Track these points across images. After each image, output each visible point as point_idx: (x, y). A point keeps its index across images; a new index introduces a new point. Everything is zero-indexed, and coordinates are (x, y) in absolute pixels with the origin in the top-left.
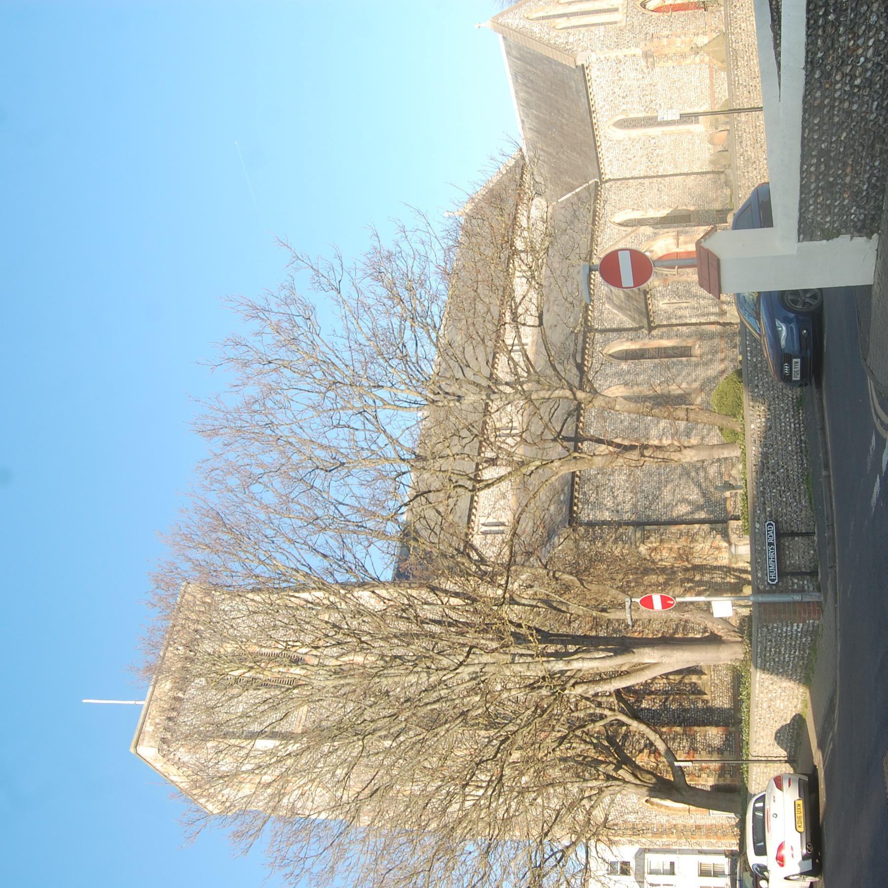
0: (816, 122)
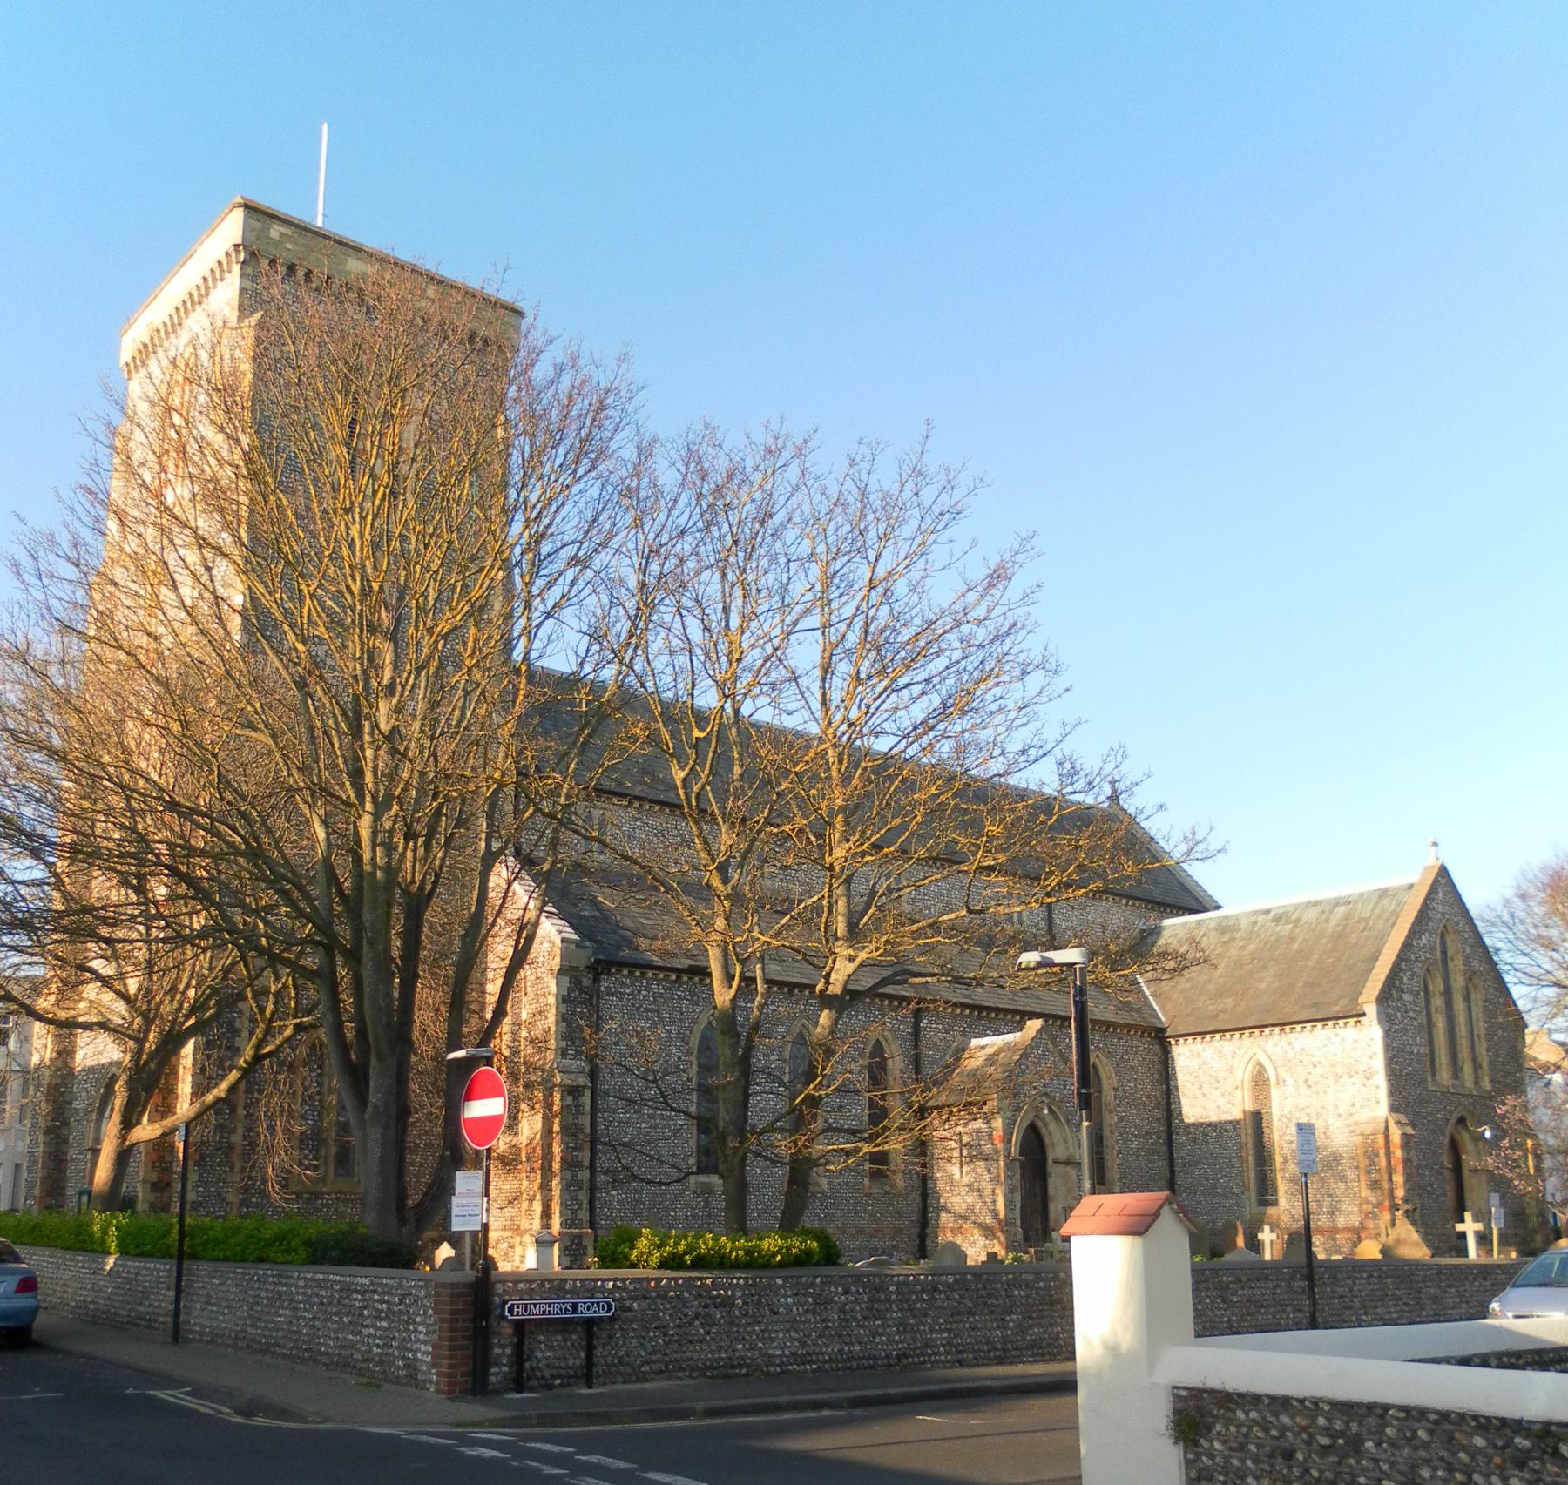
0: (1421, 1433)
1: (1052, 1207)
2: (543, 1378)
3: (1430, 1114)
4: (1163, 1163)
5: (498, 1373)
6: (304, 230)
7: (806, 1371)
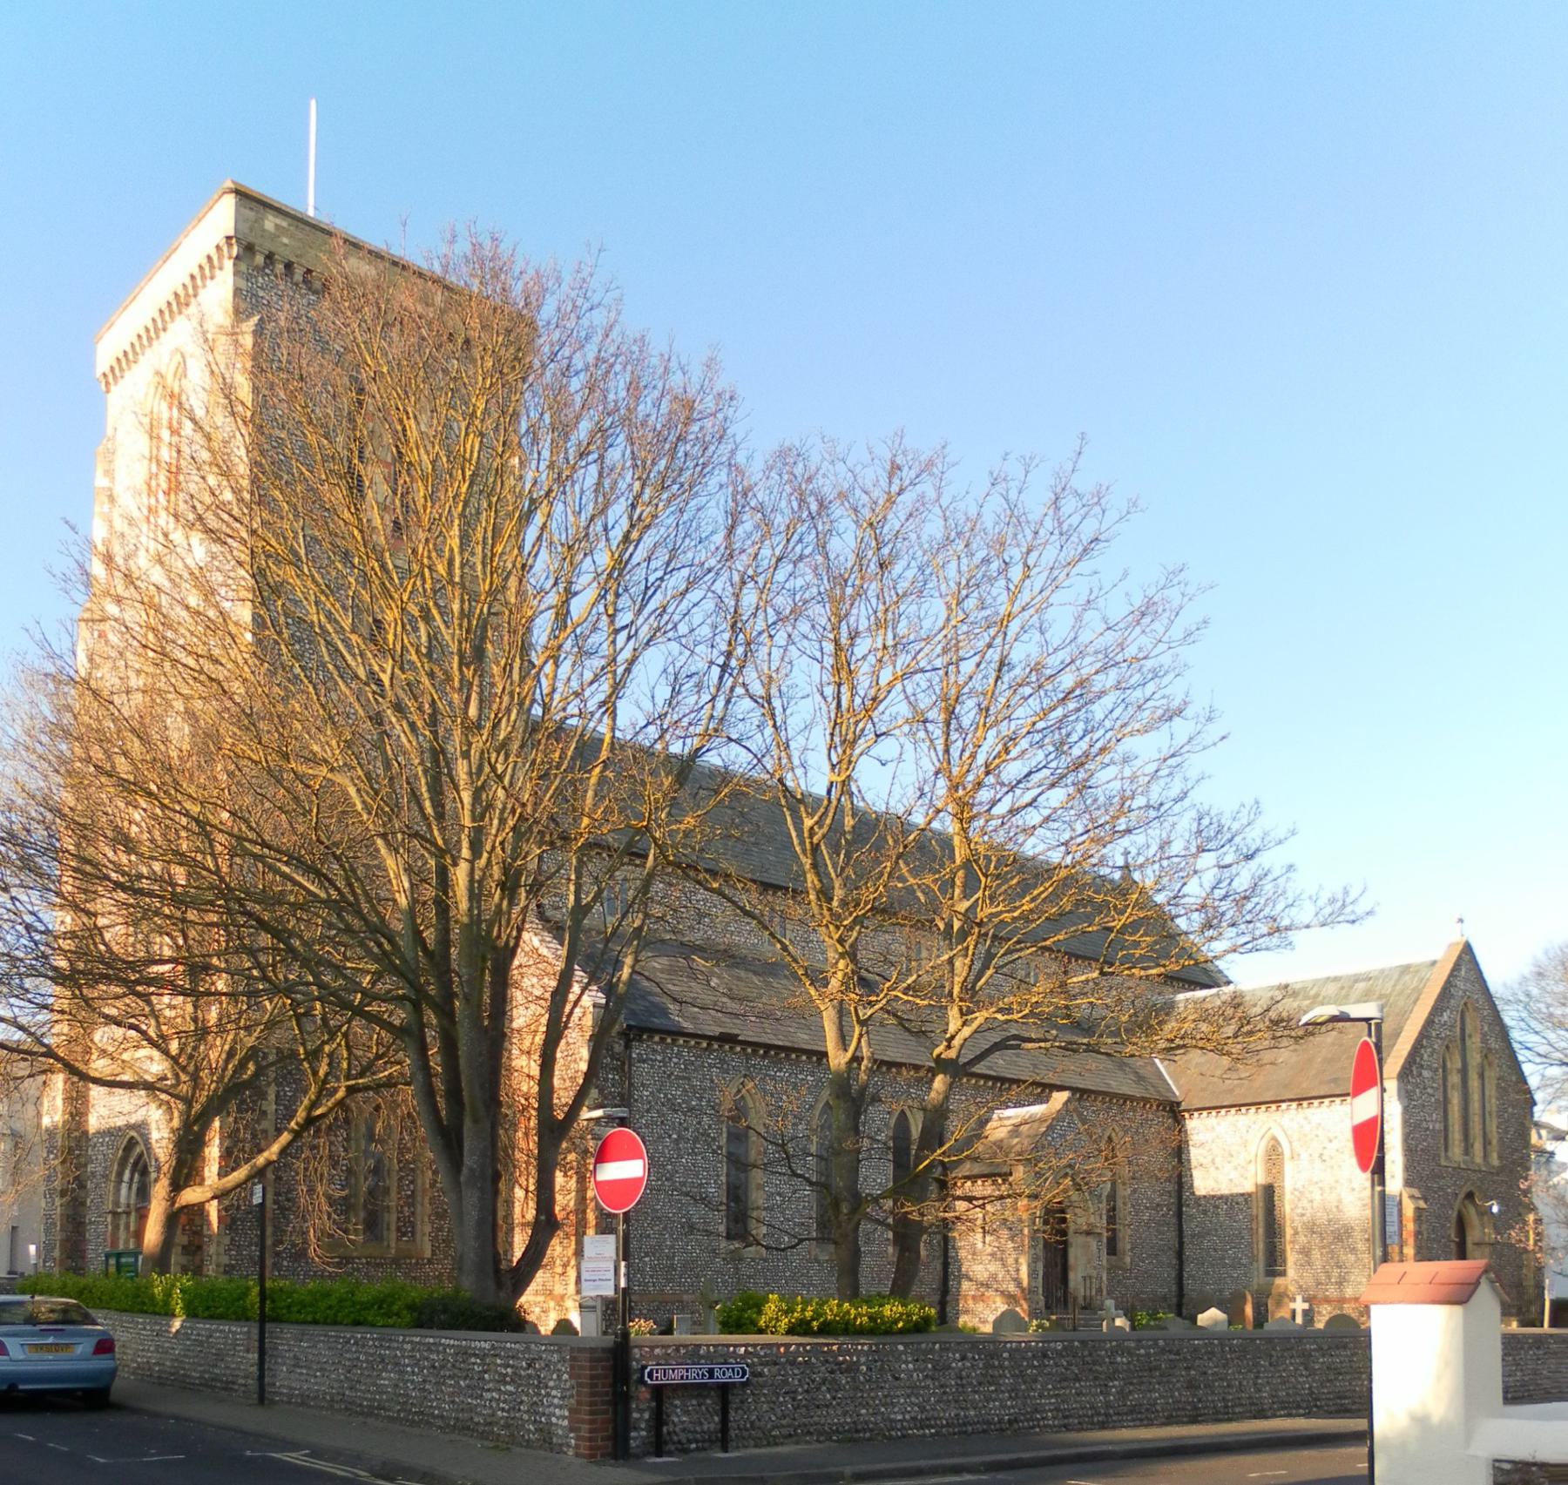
1: (1071, 1276)
2: (679, 1442)
3: (1440, 1188)
4: (1171, 1235)
5: (639, 1436)
6: (299, 220)
7: (924, 1435)
